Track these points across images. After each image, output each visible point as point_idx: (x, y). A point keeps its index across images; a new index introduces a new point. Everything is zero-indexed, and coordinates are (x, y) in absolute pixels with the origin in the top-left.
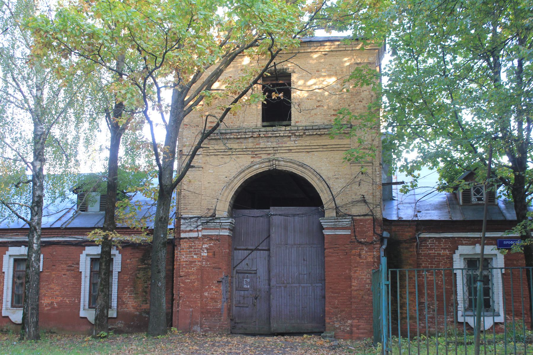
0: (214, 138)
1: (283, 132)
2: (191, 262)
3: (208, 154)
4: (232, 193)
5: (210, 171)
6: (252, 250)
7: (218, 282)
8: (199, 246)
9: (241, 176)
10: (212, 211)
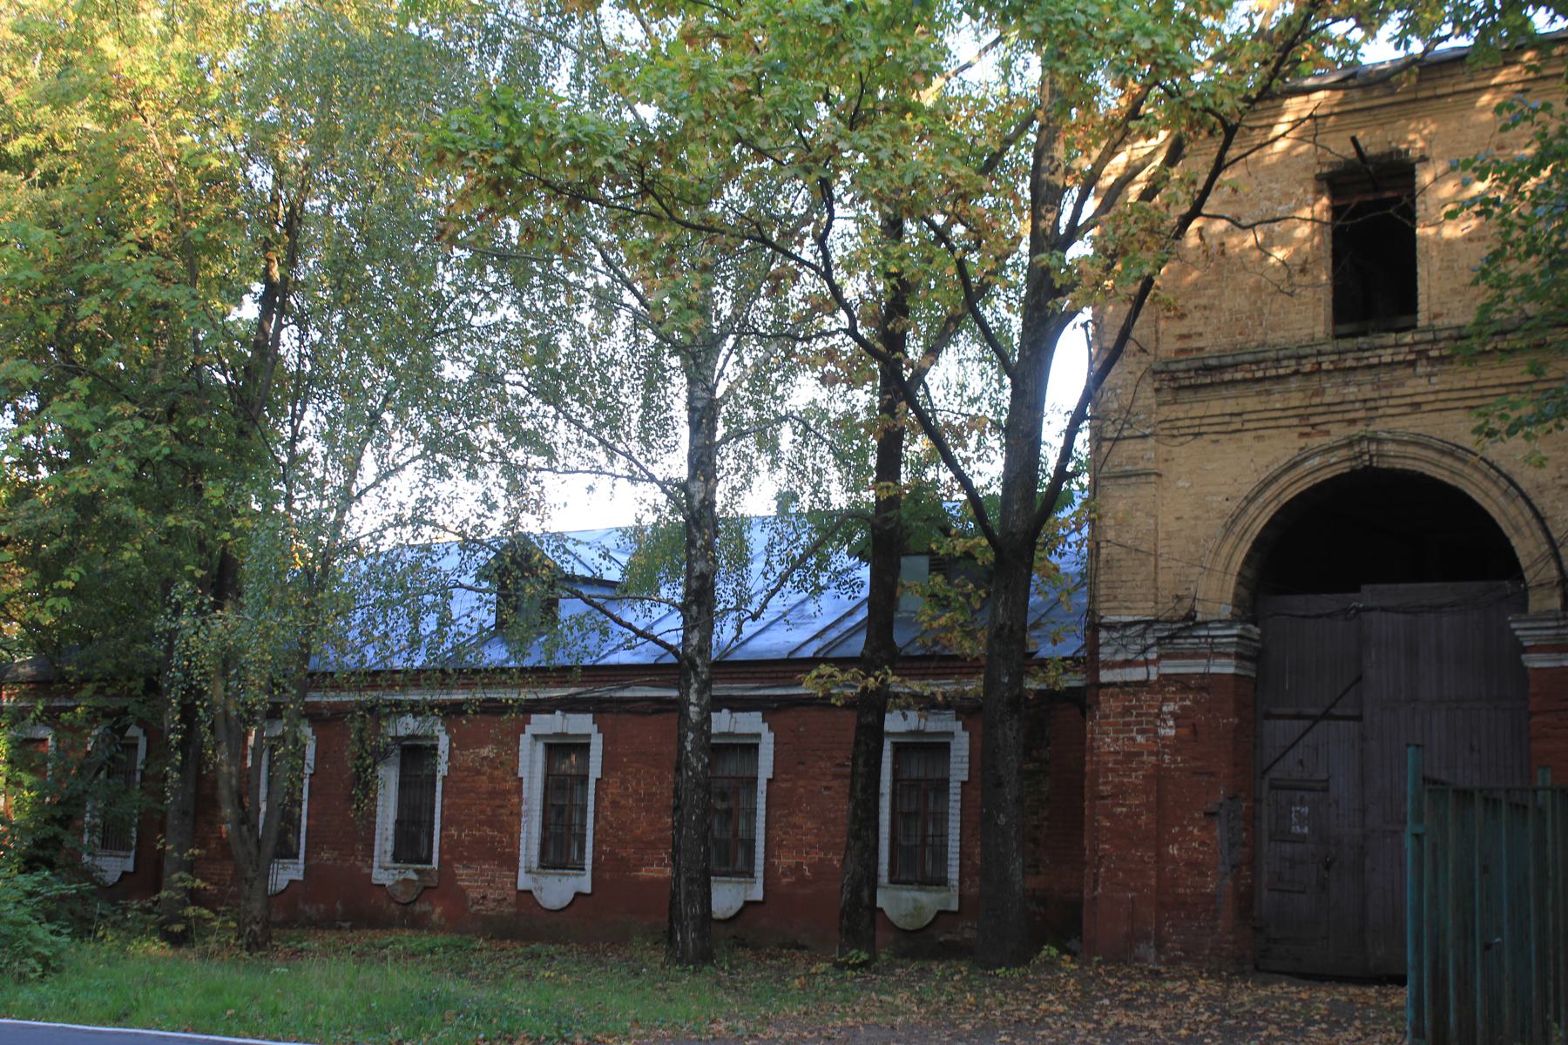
0: (1187, 383)
1: (1390, 351)
2: (1130, 756)
3: (1175, 432)
4: (1245, 547)
5: (1180, 484)
6: (1316, 719)
7: (1206, 814)
8: (1150, 706)
9: (1268, 494)
10: (1187, 603)
